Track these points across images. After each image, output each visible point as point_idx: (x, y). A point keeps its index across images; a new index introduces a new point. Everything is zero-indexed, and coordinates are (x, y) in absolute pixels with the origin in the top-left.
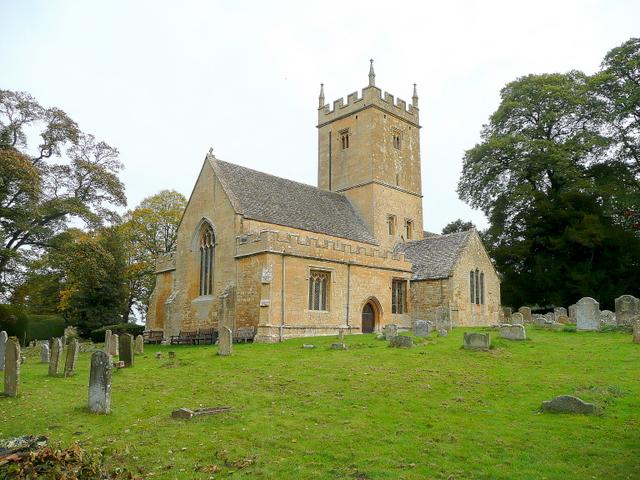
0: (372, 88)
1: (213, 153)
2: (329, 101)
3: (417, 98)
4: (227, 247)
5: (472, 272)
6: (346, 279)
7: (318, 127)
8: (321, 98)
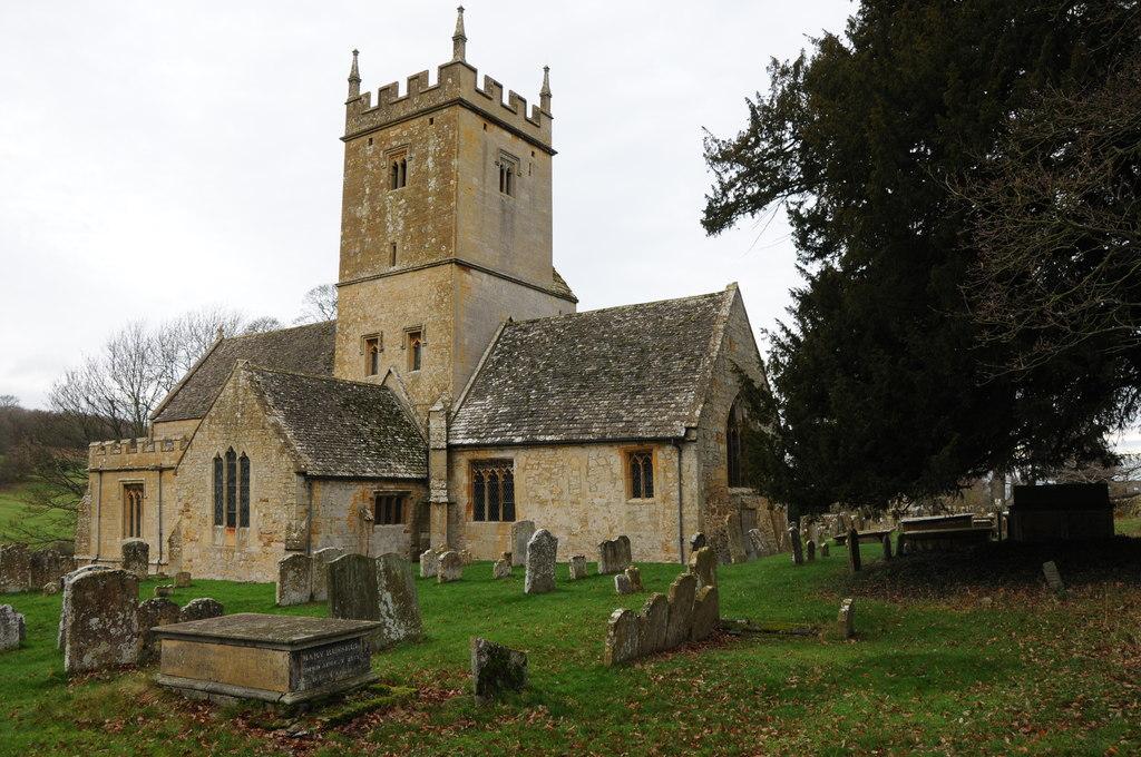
0: (456, 69)
2: (371, 86)
3: (549, 96)
5: (217, 460)
8: (355, 80)
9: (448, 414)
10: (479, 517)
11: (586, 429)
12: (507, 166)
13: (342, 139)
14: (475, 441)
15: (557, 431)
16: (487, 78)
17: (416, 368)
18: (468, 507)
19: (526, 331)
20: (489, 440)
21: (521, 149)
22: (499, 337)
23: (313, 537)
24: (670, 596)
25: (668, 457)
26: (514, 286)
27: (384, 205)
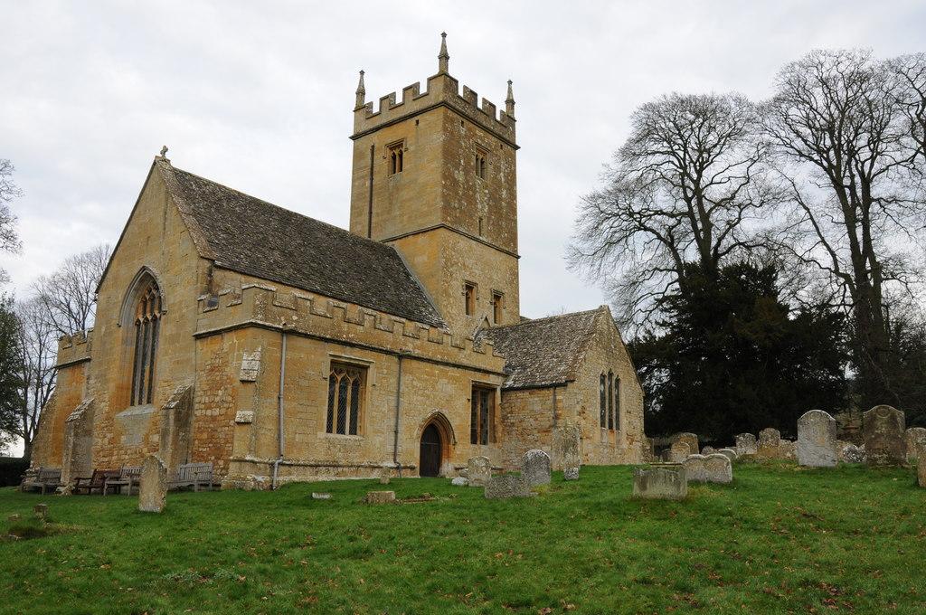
0: (445, 79)
1: (168, 156)
2: (373, 97)
4: (182, 316)
5: (603, 376)
6: (393, 380)
7: (353, 138)
8: (361, 93)
12: (481, 156)
13: (351, 138)
16: (465, 87)
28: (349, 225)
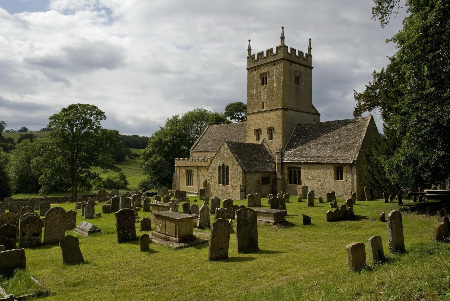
0: (283, 47)
5: (219, 167)
8: (249, 50)
9: (281, 153)
10: (291, 183)
11: (323, 159)
14: (290, 161)
15: (314, 160)
16: (291, 48)
17: (272, 139)
18: (288, 180)
19: (304, 127)
20: (294, 162)
21: (302, 69)
22: (296, 129)
23: (247, 188)
24: (340, 209)
25: (347, 169)
26: (300, 113)
27: (260, 90)
28: (72, 204)
